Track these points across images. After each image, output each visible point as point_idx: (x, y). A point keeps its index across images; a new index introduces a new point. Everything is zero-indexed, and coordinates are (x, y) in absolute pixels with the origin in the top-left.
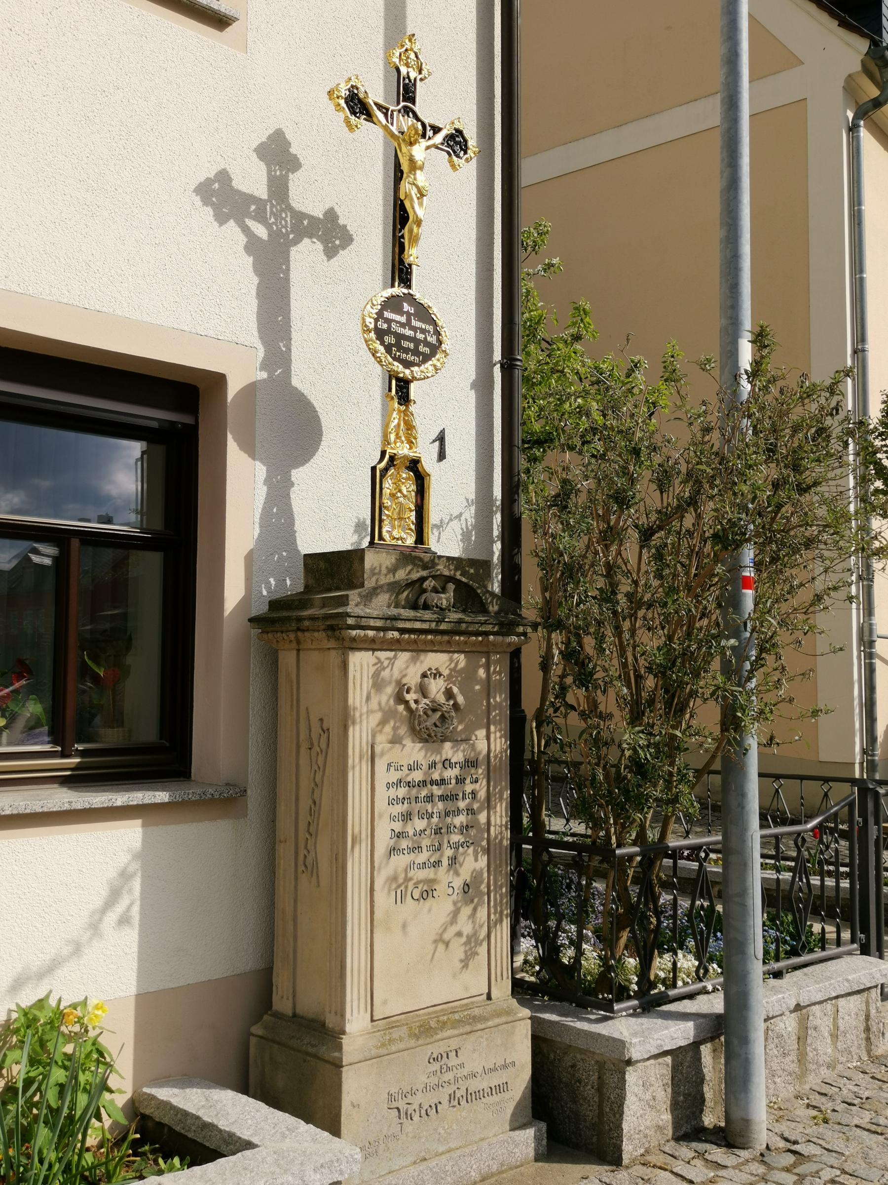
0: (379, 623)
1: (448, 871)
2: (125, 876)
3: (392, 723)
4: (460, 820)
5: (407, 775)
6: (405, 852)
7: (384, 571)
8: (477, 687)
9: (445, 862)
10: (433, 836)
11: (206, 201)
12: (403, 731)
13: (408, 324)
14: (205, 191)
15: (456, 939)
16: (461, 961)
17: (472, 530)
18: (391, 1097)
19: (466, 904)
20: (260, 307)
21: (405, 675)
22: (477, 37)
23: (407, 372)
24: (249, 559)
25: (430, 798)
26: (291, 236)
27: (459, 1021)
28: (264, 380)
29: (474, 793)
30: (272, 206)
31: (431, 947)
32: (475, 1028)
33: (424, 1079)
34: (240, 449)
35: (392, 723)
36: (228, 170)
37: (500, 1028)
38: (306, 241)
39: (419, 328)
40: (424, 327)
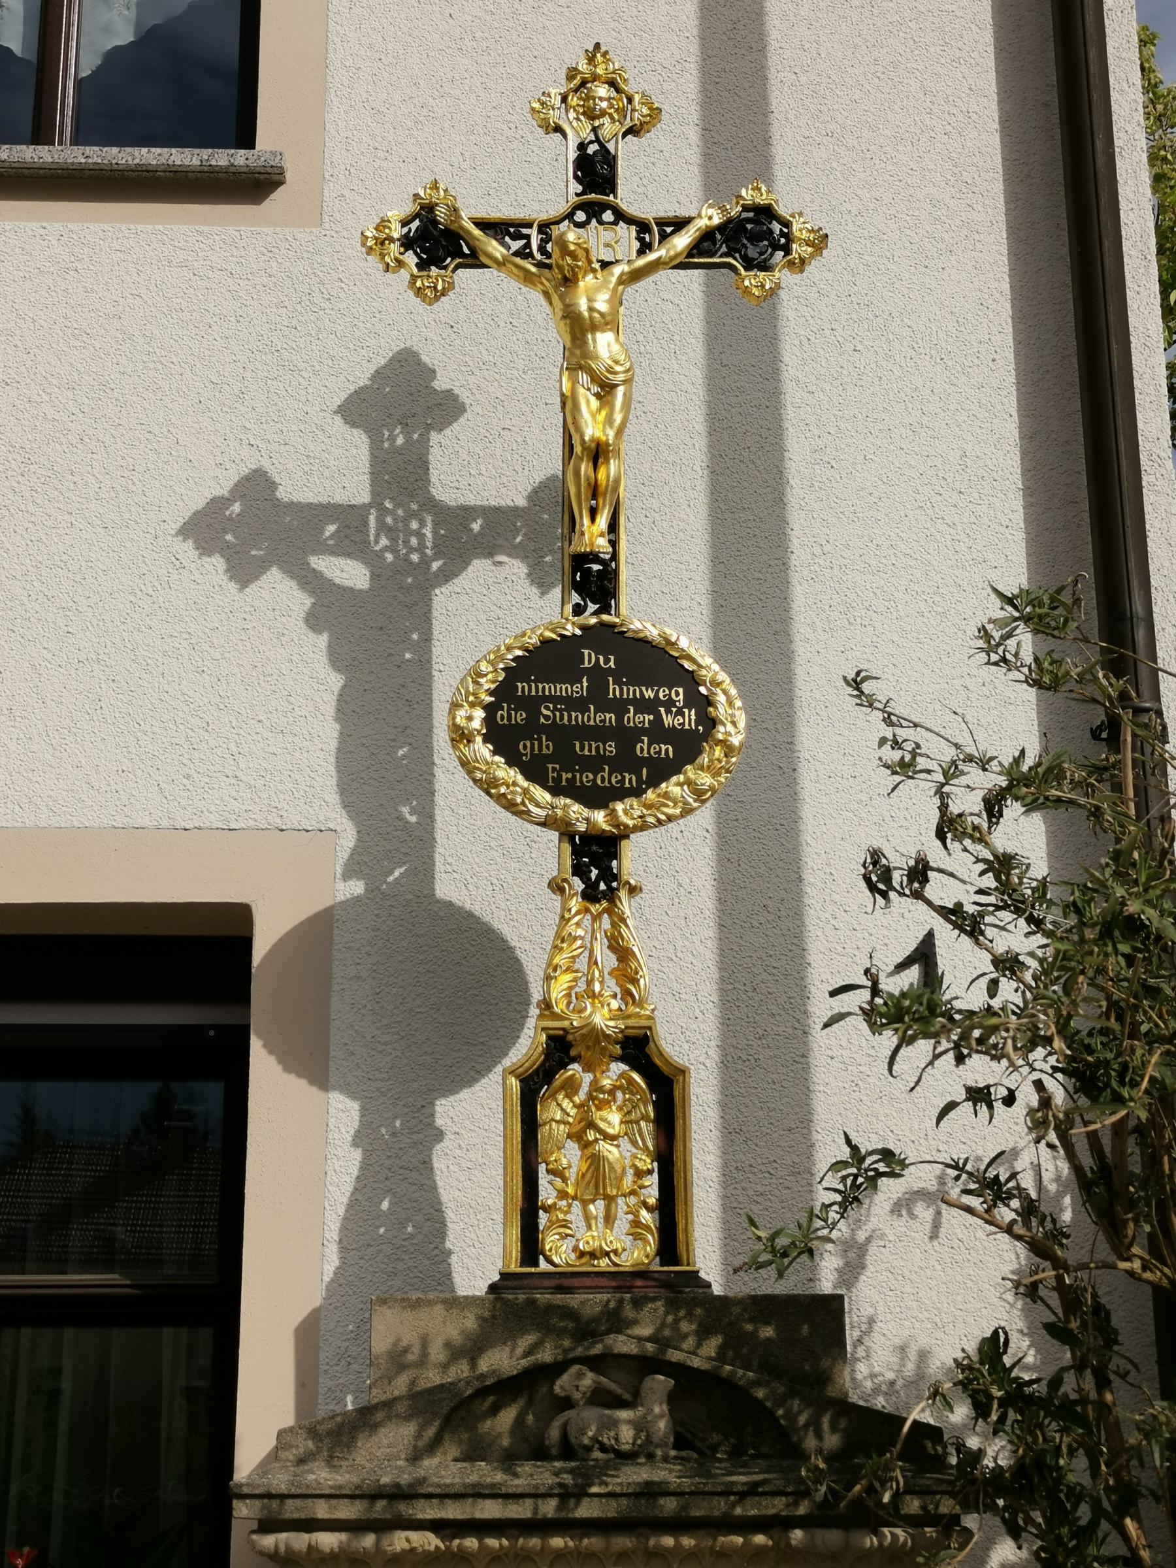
0: (347, 1511)
7: (437, 1353)
11: (205, 549)
13: (598, 697)
14: (206, 528)
17: (1060, 1195)
20: (344, 737)
23: (599, 816)
24: (309, 1335)
28: (356, 901)
30: (383, 512)
36: (267, 467)
38: (479, 567)
40: (649, 694)
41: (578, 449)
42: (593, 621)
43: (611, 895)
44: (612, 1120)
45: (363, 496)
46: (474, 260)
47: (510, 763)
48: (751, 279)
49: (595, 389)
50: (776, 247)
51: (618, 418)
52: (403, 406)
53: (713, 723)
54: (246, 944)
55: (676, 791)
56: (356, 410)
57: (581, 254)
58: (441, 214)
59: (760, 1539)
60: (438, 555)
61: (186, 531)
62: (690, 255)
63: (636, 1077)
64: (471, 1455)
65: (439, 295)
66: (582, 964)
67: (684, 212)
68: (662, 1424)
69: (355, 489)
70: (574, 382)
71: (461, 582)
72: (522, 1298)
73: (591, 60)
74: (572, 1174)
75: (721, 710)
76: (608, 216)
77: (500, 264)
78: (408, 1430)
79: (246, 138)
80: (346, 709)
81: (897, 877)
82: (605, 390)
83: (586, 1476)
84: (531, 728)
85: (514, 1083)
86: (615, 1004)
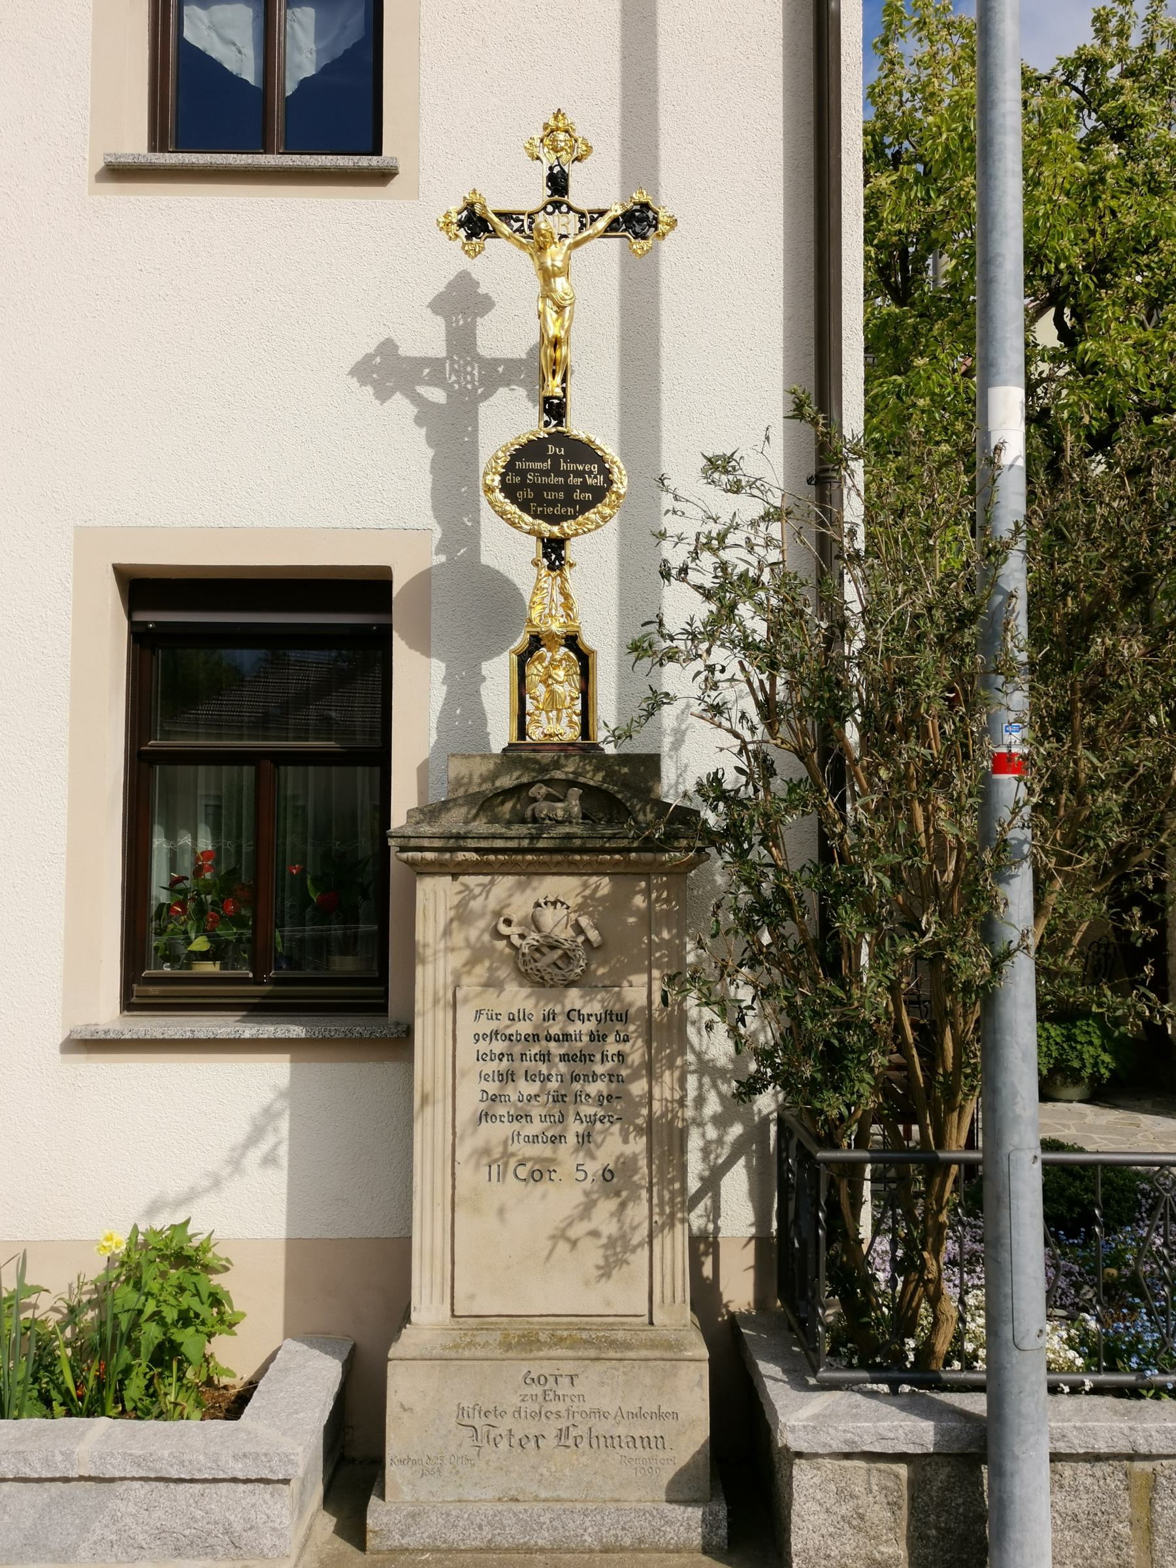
0: (437, 843)
1: (577, 1151)
2: (269, 1114)
3: (487, 963)
4: (596, 1088)
5: (507, 1027)
6: (505, 1119)
7: (476, 779)
8: (631, 920)
9: (571, 1139)
10: (550, 1104)
11: (363, 383)
12: (503, 973)
14: (363, 371)
15: (589, 1240)
16: (598, 1267)
18: (462, 1410)
19: (607, 1197)
20: (435, 482)
21: (508, 905)
22: (785, 49)
23: (556, 530)
24: (424, 770)
25: (545, 1057)
26: (480, 391)
27: (586, 1342)
28: (443, 564)
29: (621, 1056)
30: (453, 362)
31: (548, 1244)
32: (603, 1355)
33: (516, 1400)
34: (411, 647)
35: (487, 963)
36: (394, 337)
37: (650, 1363)
38: (502, 391)
40: (580, 468)
41: (546, 342)
42: (554, 430)
43: (561, 567)
44: (560, 674)
45: (442, 353)
46: (494, 234)
47: (512, 503)
48: (638, 244)
49: (555, 308)
50: (650, 226)
51: (566, 324)
52: (462, 303)
53: (611, 482)
54: (389, 584)
55: (593, 516)
56: (439, 305)
57: (548, 235)
58: (477, 208)
59: (617, 857)
60: (481, 385)
61: (352, 373)
62: (606, 231)
63: (572, 654)
64: (493, 820)
65: (477, 253)
66: (547, 601)
67: (602, 207)
68: (576, 809)
69: (438, 349)
70: (545, 305)
71: (493, 400)
72: (519, 753)
73: (556, 118)
74: (541, 699)
75: (615, 476)
76: (564, 208)
77: (508, 238)
78: (464, 810)
79: (377, 150)
80: (437, 467)
81: (674, 572)
82: (560, 309)
83: (541, 830)
84: (523, 485)
85: (515, 658)
86: (562, 620)
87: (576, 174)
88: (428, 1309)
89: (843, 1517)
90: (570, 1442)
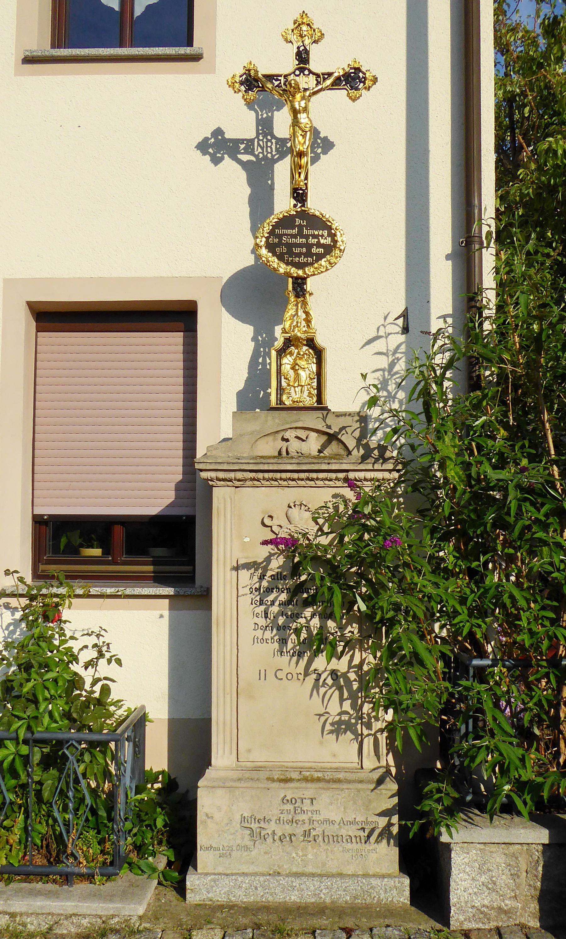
6: (269, 642)
18: (243, 819)
23: (300, 272)
33: (276, 812)
39: (310, 235)
40: (316, 233)
42: (299, 210)
43: (304, 296)
50: (361, 82)
58: (252, 73)
63: (310, 351)
76: (306, 72)
79: (190, 43)
87: (315, 52)
88: (221, 757)
89: (483, 882)
90: (311, 839)
